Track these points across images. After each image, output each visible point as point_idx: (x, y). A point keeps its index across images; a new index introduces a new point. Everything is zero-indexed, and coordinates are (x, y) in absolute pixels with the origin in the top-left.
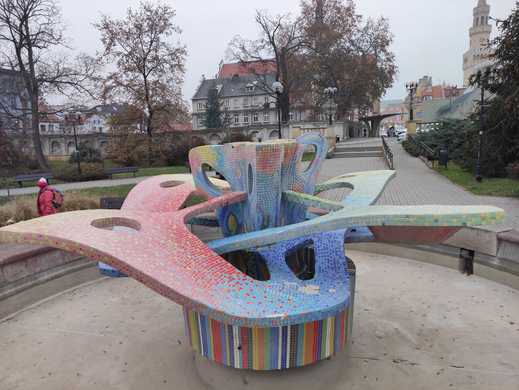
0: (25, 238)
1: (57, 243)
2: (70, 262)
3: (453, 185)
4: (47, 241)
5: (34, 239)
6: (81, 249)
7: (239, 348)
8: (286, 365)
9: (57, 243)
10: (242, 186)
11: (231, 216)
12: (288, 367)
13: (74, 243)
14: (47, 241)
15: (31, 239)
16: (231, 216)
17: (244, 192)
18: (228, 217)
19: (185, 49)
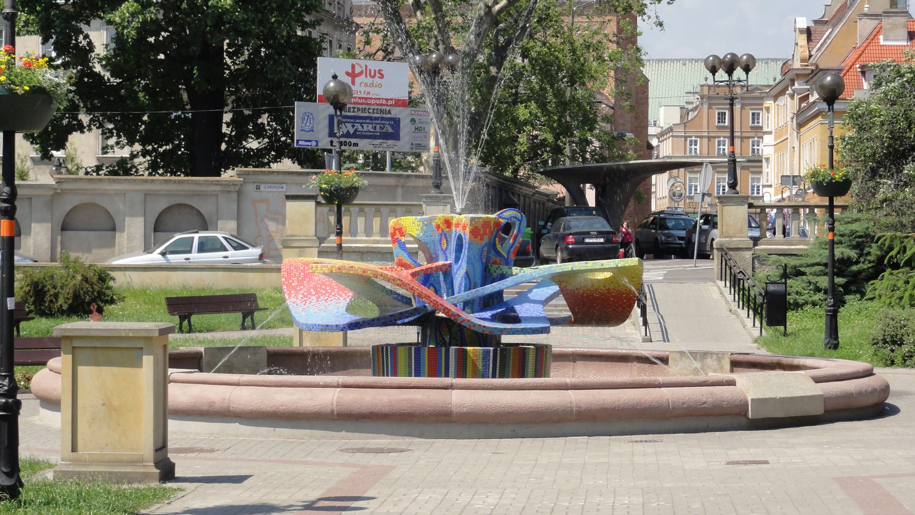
17: (448, 262)
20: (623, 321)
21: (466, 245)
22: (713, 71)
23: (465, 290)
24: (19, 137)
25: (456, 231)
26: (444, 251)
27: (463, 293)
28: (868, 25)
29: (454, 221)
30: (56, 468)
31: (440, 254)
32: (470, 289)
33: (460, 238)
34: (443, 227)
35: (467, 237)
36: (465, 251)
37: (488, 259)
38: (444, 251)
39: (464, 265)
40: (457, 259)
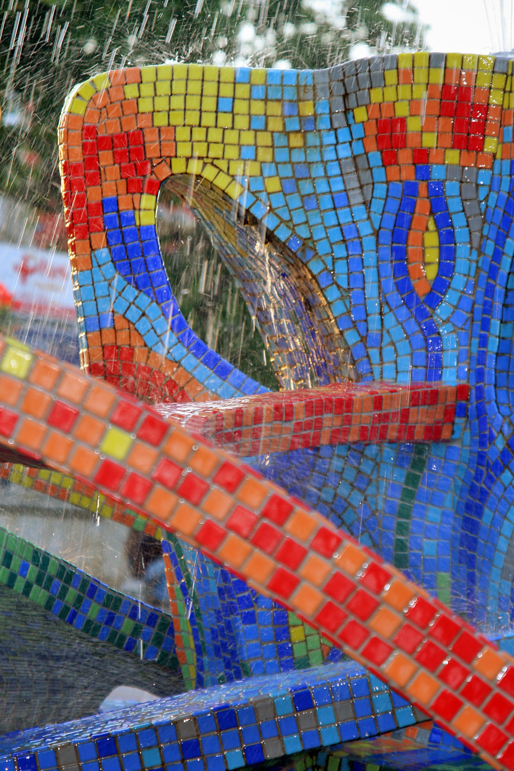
34: (424, 131)
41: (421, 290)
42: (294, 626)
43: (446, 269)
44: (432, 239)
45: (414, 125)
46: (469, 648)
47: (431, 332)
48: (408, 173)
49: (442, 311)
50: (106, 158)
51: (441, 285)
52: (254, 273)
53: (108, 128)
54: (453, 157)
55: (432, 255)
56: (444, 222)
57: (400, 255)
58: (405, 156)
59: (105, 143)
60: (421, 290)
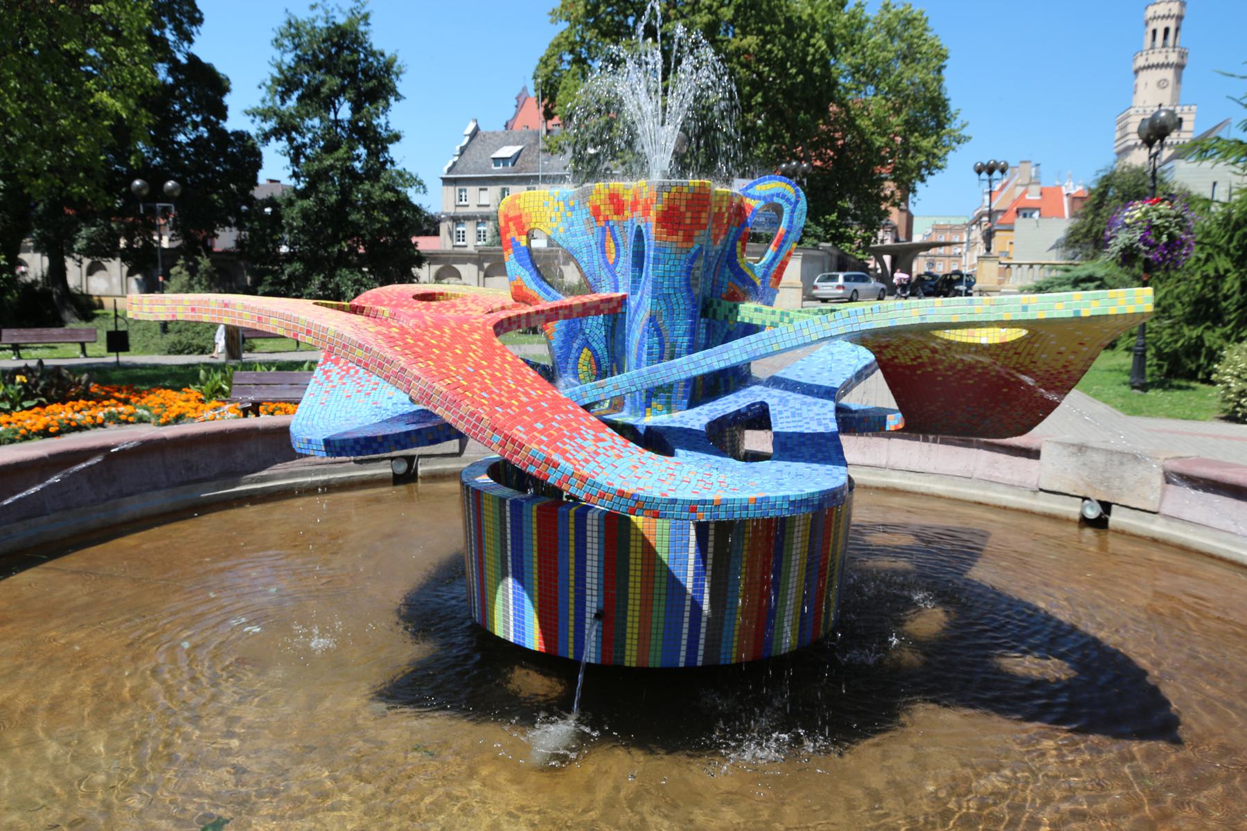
0: (193, 310)
1: (260, 318)
2: (182, 483)
3: (1193, 492)
4: (240, 315)
5: (213, 311)
6: (308, 332)
7: (598, 616)
8: (696, 659)
9: (260, 318)
10: (616, 281)
11: (585, 350)
12: (700, 661)
13: (297, 320)
14: (240, 315)
15: (207, 311)
16: (585, 350)
17: (620, 294)
18: (580, 350)
19: (269, 83)
20: (709, 423)
21: (650, 253)
22: (979, 172)
23: (651, 361)
24: (1024, 332)
25: (633, 219)
26: (611, 269)
27: (644, 369)
28: (1022, 189)
29: (628, 198)
30: (451, 751)
31: (604, 274)
32: (661, 358)
33: (639, 236)
34: (606, 210)
35: (652, 231)
36: (649, 266)
37: (716, 286)
38: (611, 269)
39: (648, 301)
40: (635, 282)
41: (611, 261)
42: (861, 375)
43: (618, 256)
44: (612, 245)
45: (602, 208)
46: (459, 406)
47: (614, 276)
48: (603, 224)
49: (618, 269)
50: (511, 224)
51: (616, 262)
52: (704, 562)
53: (512, 214)
54: (615, 217)
55: (613, 251)
56: (615, 239)
57: (604, 252)
58: (601, 218)
59: (511, 219)
60: (611, 261)
